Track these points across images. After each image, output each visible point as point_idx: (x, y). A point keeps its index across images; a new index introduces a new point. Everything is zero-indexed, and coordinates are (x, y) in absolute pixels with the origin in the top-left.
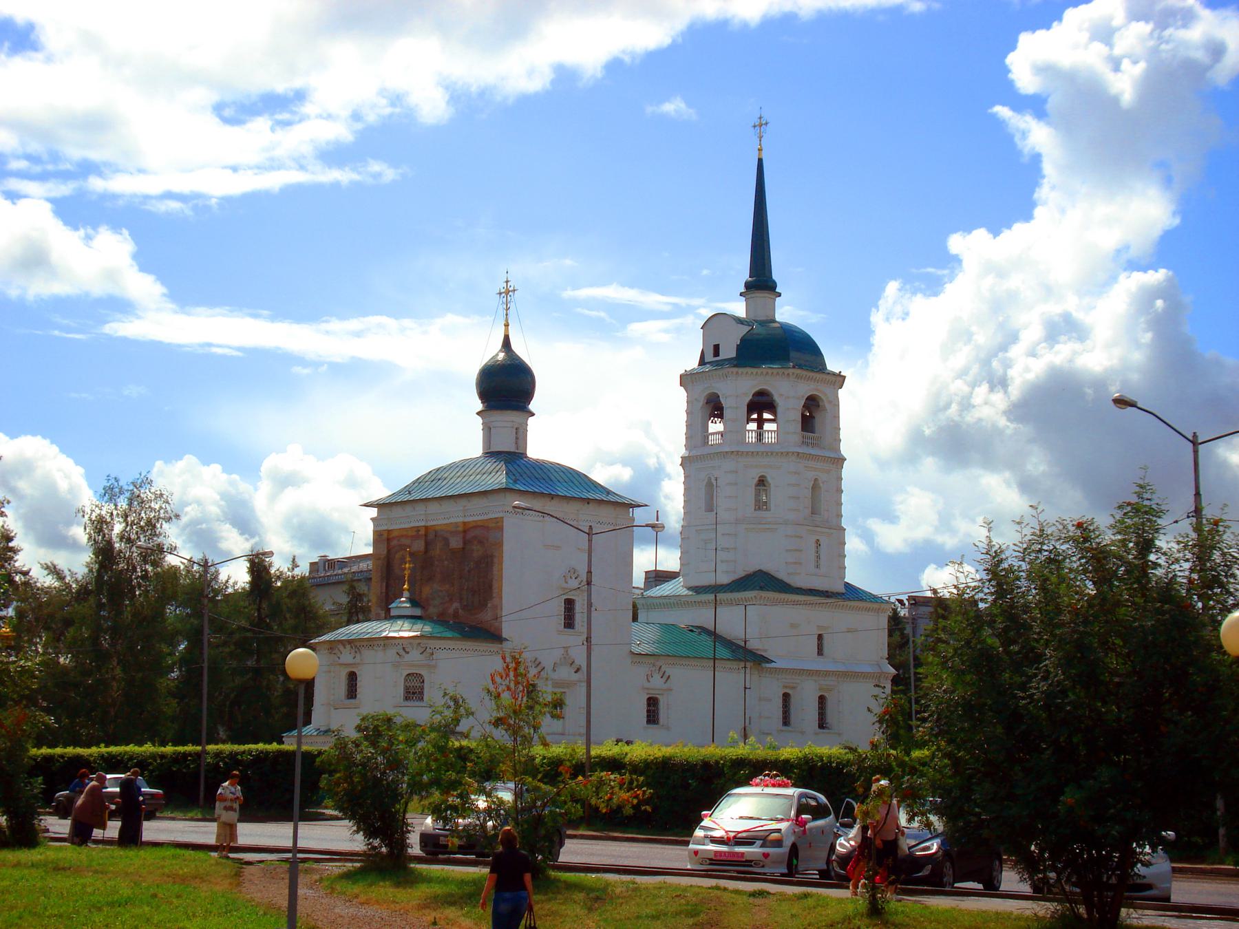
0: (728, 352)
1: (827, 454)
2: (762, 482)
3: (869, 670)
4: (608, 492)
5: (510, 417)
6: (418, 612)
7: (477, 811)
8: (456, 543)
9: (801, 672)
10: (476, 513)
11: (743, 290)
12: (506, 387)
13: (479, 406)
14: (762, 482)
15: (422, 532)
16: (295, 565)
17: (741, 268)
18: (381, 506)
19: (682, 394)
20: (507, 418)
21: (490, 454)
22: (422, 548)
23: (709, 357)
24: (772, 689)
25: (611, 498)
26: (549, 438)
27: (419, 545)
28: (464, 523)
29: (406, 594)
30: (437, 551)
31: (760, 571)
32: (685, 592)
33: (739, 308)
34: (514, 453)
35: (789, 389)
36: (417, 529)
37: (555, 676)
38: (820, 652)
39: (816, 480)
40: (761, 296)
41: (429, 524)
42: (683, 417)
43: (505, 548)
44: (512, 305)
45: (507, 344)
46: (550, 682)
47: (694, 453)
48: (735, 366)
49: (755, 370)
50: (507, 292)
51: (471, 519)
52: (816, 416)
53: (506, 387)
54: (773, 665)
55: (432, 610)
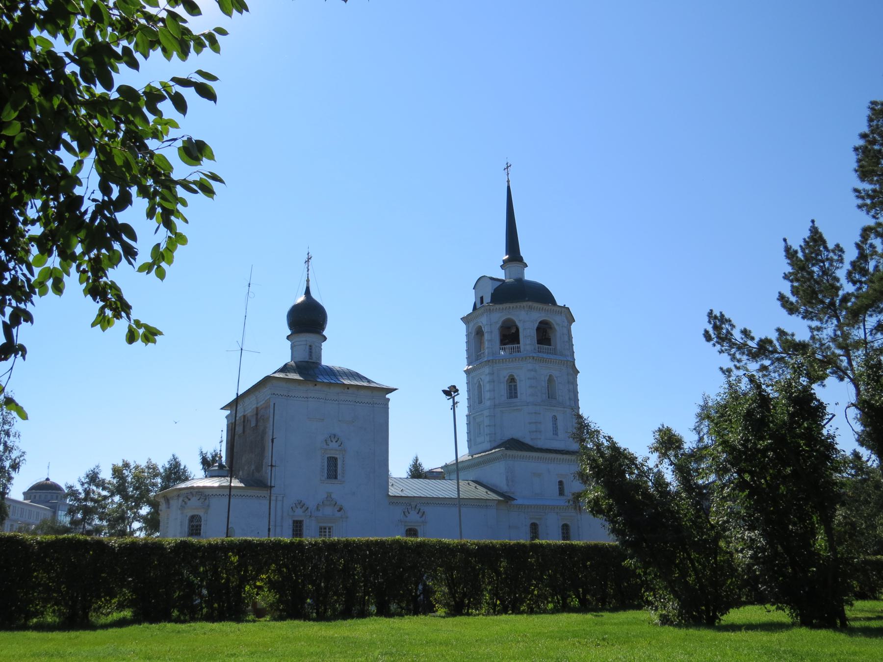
0: (488, 299)
1: (562, 358)
2: (512, 380)
4: (369, 381)
7: (201, 603)
12: (307, 319)
16: (298, 528)
19: (463, 327)
35: (527, 319)
39: (550, 376)
40: (515, 266)
45: (308, 292)
53: (307, 319)
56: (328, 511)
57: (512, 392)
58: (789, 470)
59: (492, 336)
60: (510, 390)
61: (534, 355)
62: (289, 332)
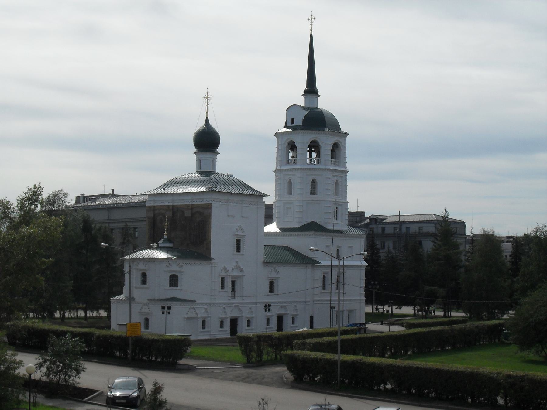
0: (299, 122)
6: (171, 245)
8: (188, 214)
13: (194, 150)
15: (171, 208)
17: (303, 86)
20: (207, 156)
23: (290, 124)
24: (319, 274)
25: (254, 193)
26: (225, 162)
32: (278, 230)
35: (326, 141)
36: (169, 206)
39: (337, 181)
42: (275, 150)
48: (303, 129)
50: (208, 98)
51: (195, 203)
54: (320, 264)
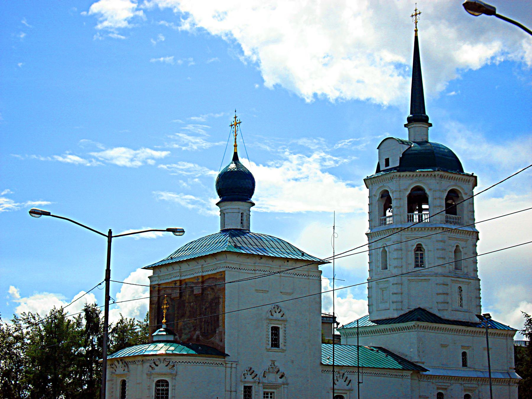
0: (395, 163)
2: (419, 248)
3: (501, 376)
5: (239, 205)
9: (450, 378)
10: (210, 269)
11: (406, 122)
14: (419, 248)
18: (153, 268)
21: (223, 231)
22: (178, 295)
27: (176, 294)
28: (203, 277)
29: (164, 326)
30: (187, 296)
31: (419, 308)
33: (404, 135)
34: (240, 230)
35: (436, 186)
37: (265, 380)
38: (465, 364)
39: (457, 246)
41: (183, 278)
43: (227, 291)
44: (238, 132)
46: (261, 385)
47: (375, 230)
48: (398, 171)
49: (412, 173)
52: (457, 206)
53: (236, 187)
54: (427, 373)
55: (184, 337)
56: (272, 378)
57: (419, 262)
58: (496, 87)
59: (400, 201)
60: (416, 258)
61: (444, 226)
62: (218, 199)
